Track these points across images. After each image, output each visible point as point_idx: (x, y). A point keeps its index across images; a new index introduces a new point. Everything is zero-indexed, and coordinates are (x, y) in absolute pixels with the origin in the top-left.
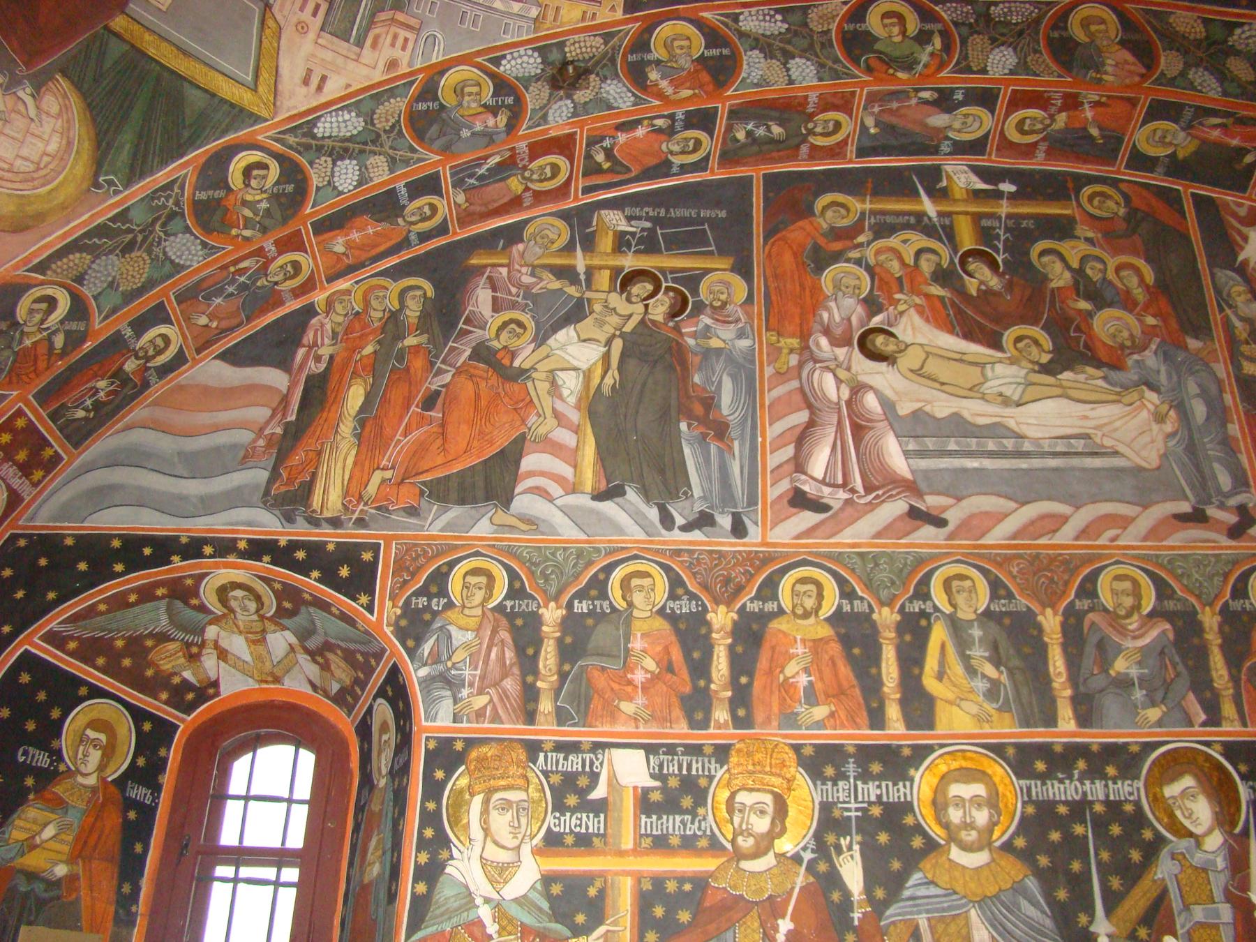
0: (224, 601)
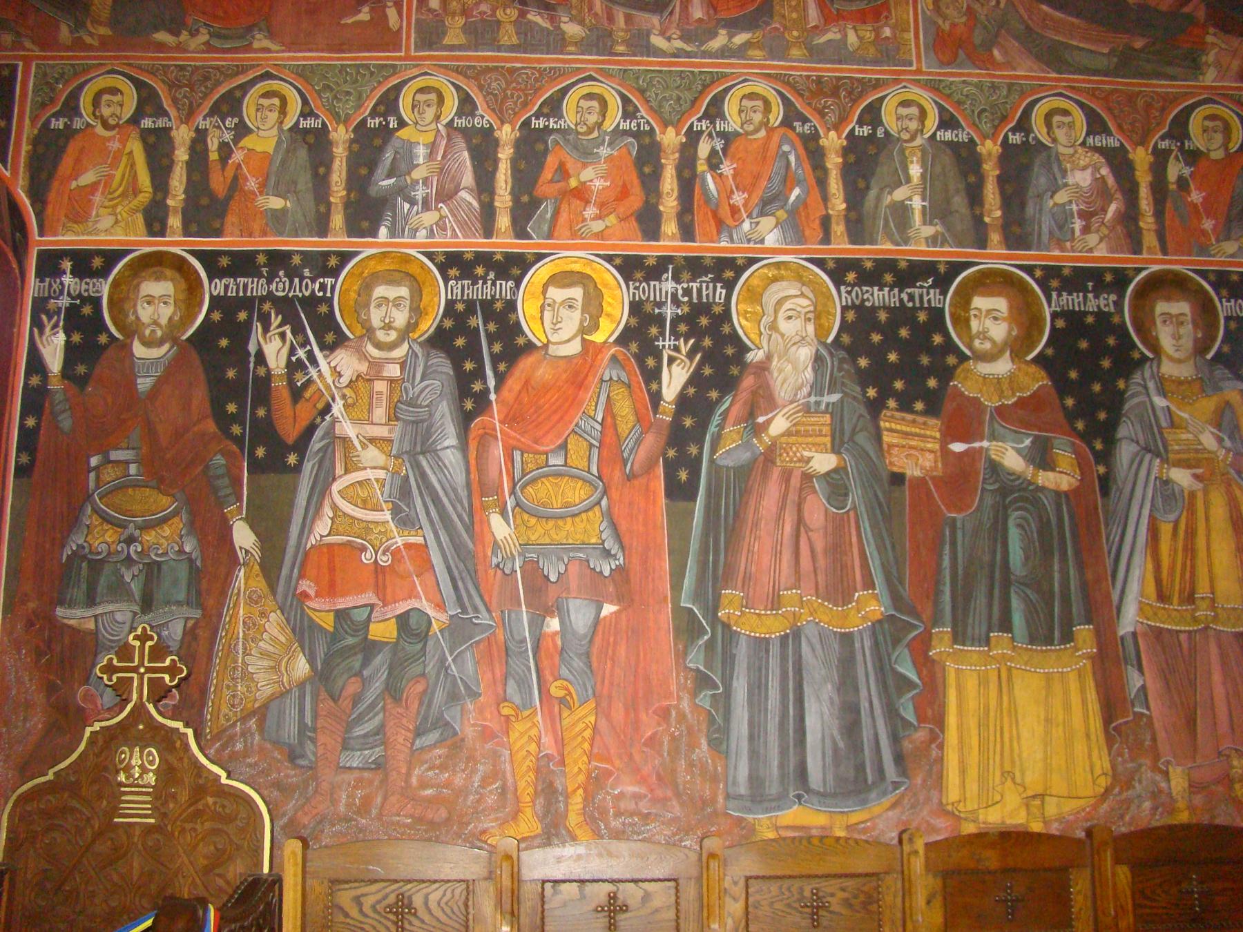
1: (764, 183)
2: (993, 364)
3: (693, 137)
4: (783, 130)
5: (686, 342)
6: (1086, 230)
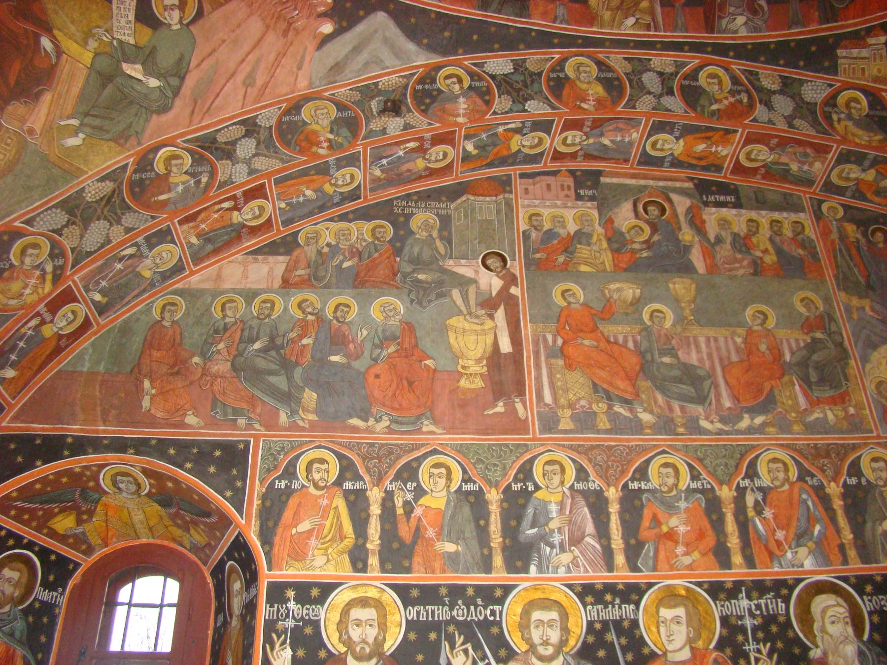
0: (115, 483)
1: (794, 523)
3: (741, 492)
4: (799, 484)
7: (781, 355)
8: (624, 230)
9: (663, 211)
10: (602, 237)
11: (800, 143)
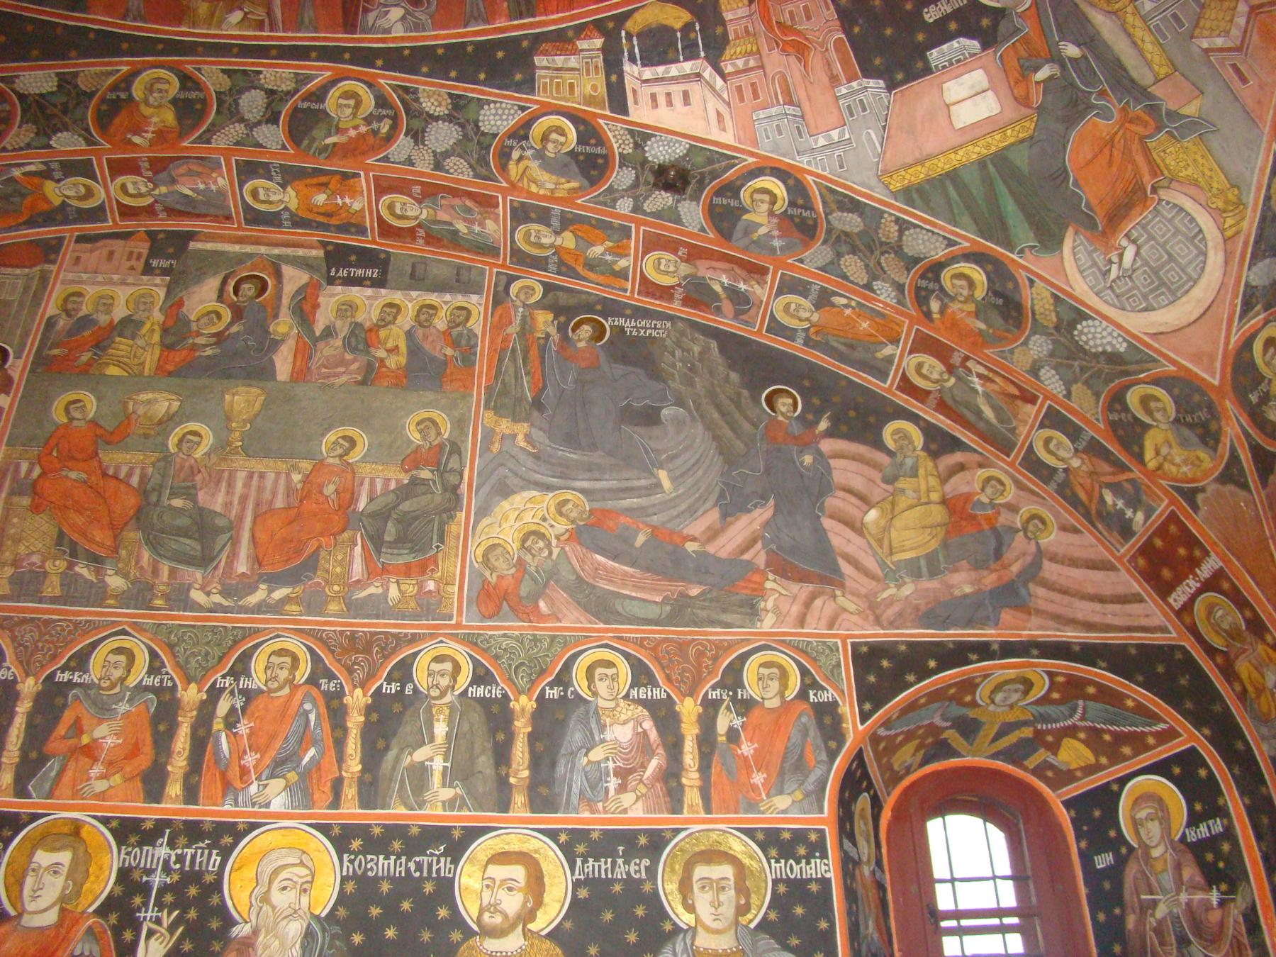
1: (278, 744)
2: (502, 940)
3: (215, 693)
4: (307, 687)
5: (169, 914)
6: (622, 788)
7: (353, 499)
8: (193, 318)
9: (263, 288)
10: (156, 328)
11: (455, 193)
